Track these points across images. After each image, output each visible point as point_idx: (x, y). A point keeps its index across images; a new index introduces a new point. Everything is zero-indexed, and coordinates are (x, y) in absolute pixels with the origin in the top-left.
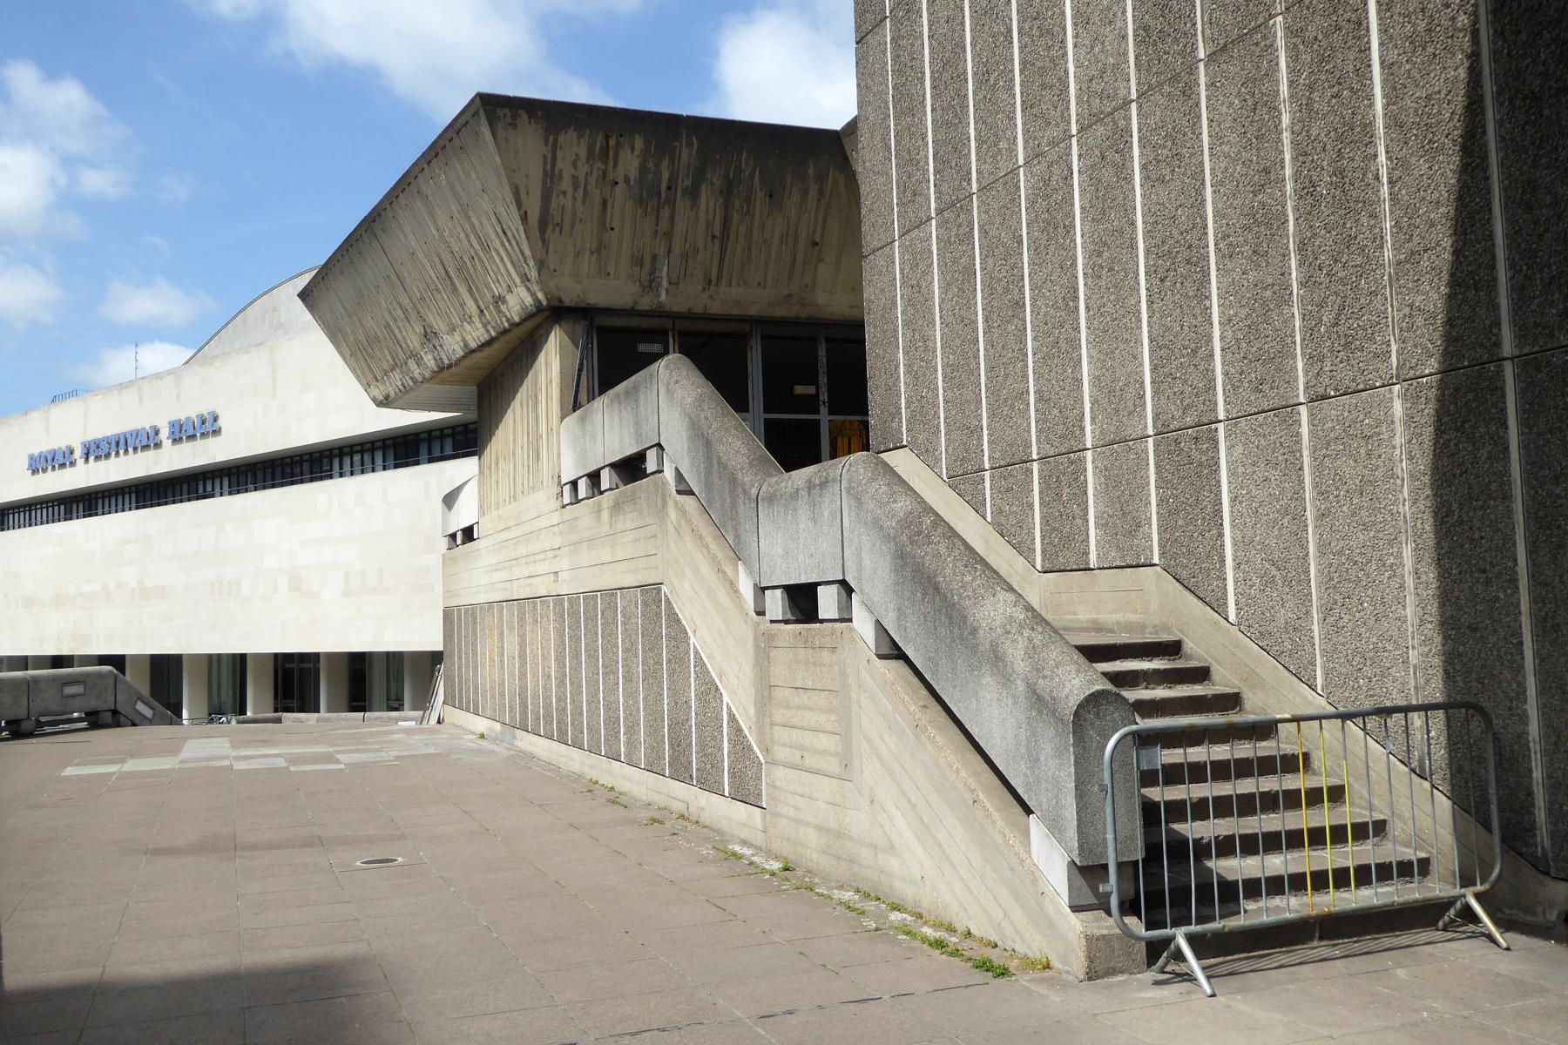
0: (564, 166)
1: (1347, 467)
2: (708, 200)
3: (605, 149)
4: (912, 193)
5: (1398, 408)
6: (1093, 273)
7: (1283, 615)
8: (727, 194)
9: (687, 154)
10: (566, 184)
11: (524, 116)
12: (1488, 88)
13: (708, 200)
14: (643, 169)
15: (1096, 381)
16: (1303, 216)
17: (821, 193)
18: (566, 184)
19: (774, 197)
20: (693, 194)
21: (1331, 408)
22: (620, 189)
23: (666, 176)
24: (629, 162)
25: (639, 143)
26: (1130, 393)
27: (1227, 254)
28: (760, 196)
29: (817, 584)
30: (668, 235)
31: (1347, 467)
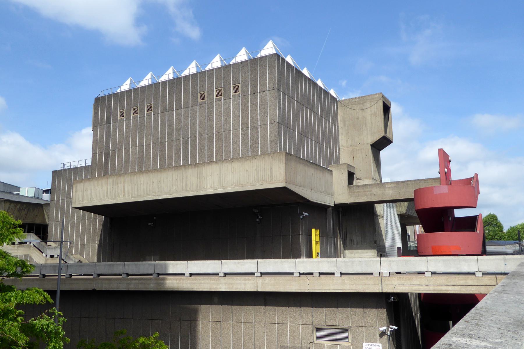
0: (11, 207)
1: (93, 249)
2: (26, 211)
3: (16, 205)
4: (57, 218)
5: (96, 245)
6: (76, 232)
7: (88, 258)
8: (28, 210)
9: (25, 206)
10: (11, 209)
11: (8, 202)
12: (246, 50)
13: (26, 211)
14: (19, 207)
15: (75, 240)
16: (92, 232)
17: (39, 210)
18: (11, 209)
19: (33, 210)
20: (24, 210)
21: (221, 131)
22: (17, 209)
23: (22, 208)
24: (18, 207)
25: (20, 205)
26: (78, 241)
27: (87, 233)
28: (32, 210)
29: (54, 255)
30: (20, 214)
31: (93, 249)
